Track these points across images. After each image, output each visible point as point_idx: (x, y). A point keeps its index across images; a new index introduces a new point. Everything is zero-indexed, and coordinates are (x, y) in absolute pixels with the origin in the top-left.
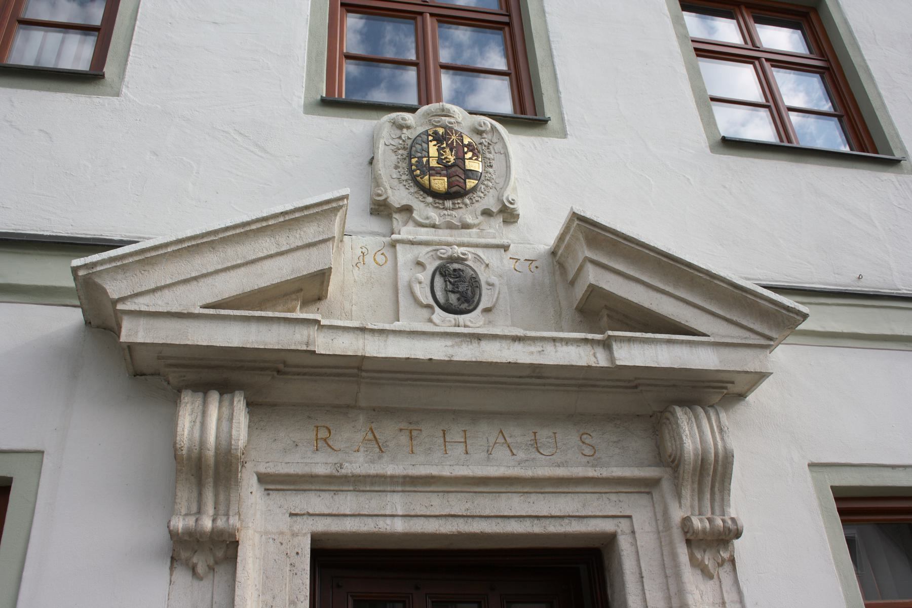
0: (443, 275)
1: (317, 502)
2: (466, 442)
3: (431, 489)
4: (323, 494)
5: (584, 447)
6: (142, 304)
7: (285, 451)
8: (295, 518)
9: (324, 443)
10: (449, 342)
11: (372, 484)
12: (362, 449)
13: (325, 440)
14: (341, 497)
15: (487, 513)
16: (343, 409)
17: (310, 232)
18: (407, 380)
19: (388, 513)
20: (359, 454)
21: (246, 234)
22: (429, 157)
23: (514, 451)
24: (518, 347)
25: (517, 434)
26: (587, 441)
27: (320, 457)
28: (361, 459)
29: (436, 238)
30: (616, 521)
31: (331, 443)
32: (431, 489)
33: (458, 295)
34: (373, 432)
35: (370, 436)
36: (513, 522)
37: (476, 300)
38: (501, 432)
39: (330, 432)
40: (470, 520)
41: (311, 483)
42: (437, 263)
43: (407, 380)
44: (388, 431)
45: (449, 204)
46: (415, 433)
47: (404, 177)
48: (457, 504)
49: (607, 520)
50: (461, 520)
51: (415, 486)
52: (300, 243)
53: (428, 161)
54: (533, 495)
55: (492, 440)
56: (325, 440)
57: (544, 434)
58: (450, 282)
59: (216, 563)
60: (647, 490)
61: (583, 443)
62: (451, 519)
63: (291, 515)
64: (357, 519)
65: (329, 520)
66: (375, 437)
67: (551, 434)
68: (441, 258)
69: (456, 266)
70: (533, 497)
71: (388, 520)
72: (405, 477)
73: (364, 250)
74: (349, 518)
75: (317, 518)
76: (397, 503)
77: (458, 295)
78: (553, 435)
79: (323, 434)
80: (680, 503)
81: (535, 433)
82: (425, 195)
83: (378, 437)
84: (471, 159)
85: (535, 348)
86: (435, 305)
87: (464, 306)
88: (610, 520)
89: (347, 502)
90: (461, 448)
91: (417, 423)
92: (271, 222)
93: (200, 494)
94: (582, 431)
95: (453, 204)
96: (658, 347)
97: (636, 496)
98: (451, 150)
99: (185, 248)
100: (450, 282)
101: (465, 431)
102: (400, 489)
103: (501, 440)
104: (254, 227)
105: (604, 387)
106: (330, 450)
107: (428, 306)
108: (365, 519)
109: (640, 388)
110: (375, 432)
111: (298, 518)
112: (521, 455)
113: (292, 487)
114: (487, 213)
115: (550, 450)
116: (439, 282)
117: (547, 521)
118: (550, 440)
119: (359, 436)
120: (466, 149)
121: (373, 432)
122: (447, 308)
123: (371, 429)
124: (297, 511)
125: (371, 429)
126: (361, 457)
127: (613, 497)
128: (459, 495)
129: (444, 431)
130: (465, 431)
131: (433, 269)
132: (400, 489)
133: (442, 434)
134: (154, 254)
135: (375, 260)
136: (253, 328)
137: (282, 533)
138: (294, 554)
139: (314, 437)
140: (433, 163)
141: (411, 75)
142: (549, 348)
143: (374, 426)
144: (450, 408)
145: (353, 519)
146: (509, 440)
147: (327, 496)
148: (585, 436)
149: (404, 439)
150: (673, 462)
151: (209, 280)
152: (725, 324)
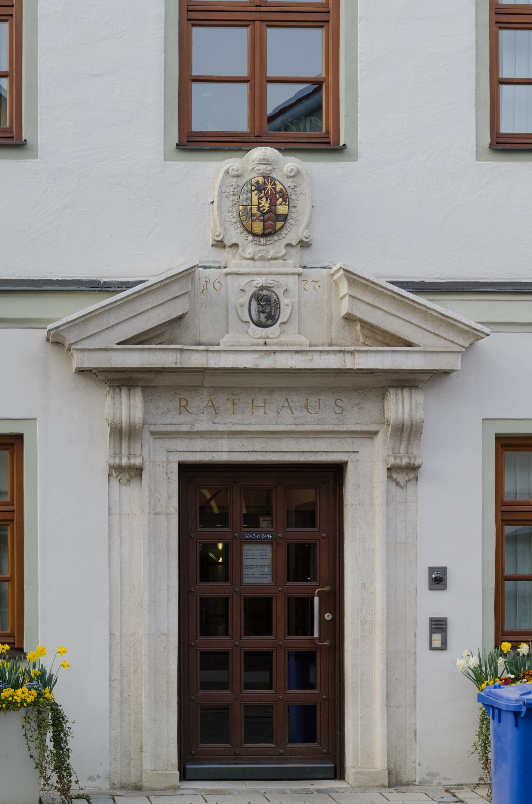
0: (257, 300)
1: (181, 444)
2: (265, 406)
3: (244, 436)
4: (184, 440)
5: (337, 408)
6: (86, 345)
7: (163, 414)
8: (170, 453)
9: (183, 409)
10: (256, 356)
11: (211, 434)
12: (205, 412)
13: (185, 407)
14: (194, 442)
15: (275, 450)
16: (195, 388)
17: (175, 290)
18: (232, 373)
19: (219, 450)
20: (204, 415)
21: (139, 296)
22: (251, 205)
23: (294, 412)
24: (298, 357)
25: (297, 401)
26: (339, 404)
27: (183, 418)
28: (205, 418)
29: (254, 270)
30: (349, 454)
31: (188, 409)
32: (244, 436)
33: (266, 315)
34: (211, 401)
35: (210, 404)
36: (288, 454)
37: (276, 317)
38: (287, 399)
39: (187, 402)
40: (264, 453)
41: (178, 434)
42: (253, 290)
43: (232, 373)
44: (220, 400)
45: (263, 240)
46: (236, 401)
47: (234, 220)
48: (258, 444)
49: (344, 453)
50: (259, 454)
51: (235, 435)
52: (169, 298)
53: (251, 208)
54: (301, 439)
55: (281, 404)
56: (185, 407)
57: (313, 400)
58: (261, 305)
59: (131, 477)
60: (371, 436)
61: (337, 405)
62: (254, 453)
63: (168, 451)
64: (203, 454)
65: (187, 454)
66: (212, 404)
67: (317, 400)
68: (256, 287)
69: (265, 293)
70: (301, 440)
71: (219, 454)
72: (229, 431)
73: (207, 280)
74: (198, 453)
75: (181, 453)
76: (224, 444)
77: (266, 315)
78: (318, 401)
79: (184, 403)
80: (412, 422)
81: (307, 399)
82: (248, 235)
83: (214, 404)
84: (281, 204)
85: (307, 357)
86: (250, 321)
87: (270, 322)
88: (346, 453)
89: (198, 444)
90: (262, 410)
91: (237, 395)
92: (153, 288)
93: (121, 443)
94: (337, 398)
95: (266, 240)
96: (386, 355)
97: (364, 440)
98: (267, 199)
99: (106, 310)
100: (261, 305)
101: (265, 399)
102: (226, 437)
103: (286, 404)
104: (143, 292)
105: (351, 373)
106: (187, 413)
107: (247, 322)
108: (207, 453)
109: (375, 374)
110: (213, 401)
111: (172, 453)
112: (297, 414)
113: (168, 437)
114: (289, 245)
115: (315, 410)
116: (254, 304)
117: (309, 454)
118: (316, 404)
119: (204, 404)
120: (278, 196)
121: (211, 401)
122: (259, 324)
123: (211, 400)
124: (171, 450)
125: (211, 400)
126: (204, 417)
127: (349, 441)
128: (259, 440)
129: (253, 399)
130: (265, 399)
131: (250, 295)
132: (226, 437)
133: (251, 402)
134: (90, 316)
135: (214, 286)
136: (146, 354)
137: (163, 462)
138: (170, 472)
139: (179, 405)
140: (255, 211)
141: (240, 204)
142: (316, 356)
143: (212, 397)
144: (257, 386)
145: (201, 453)
146: (291, 404)
147: (186, 441)
148: (338, 401)
149: (229, 405)
150: (387, 422)
151: (120, 327)
152: (434, 337)
